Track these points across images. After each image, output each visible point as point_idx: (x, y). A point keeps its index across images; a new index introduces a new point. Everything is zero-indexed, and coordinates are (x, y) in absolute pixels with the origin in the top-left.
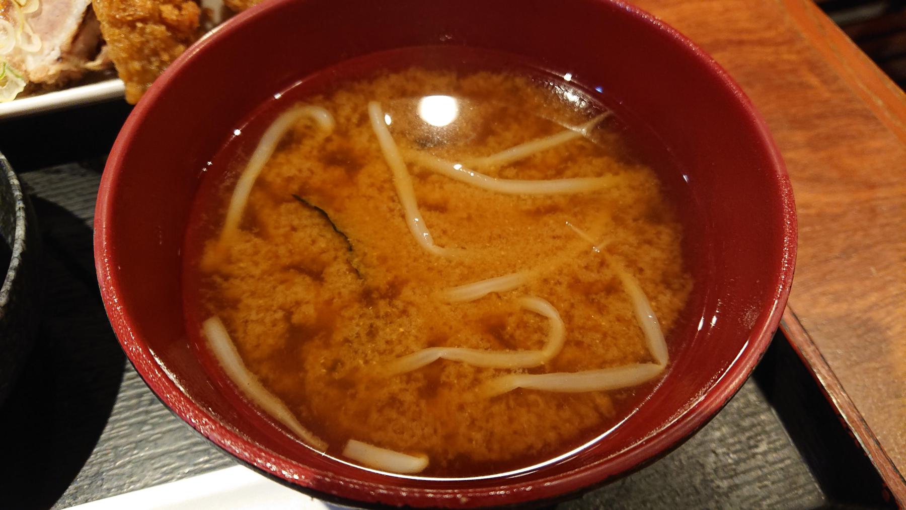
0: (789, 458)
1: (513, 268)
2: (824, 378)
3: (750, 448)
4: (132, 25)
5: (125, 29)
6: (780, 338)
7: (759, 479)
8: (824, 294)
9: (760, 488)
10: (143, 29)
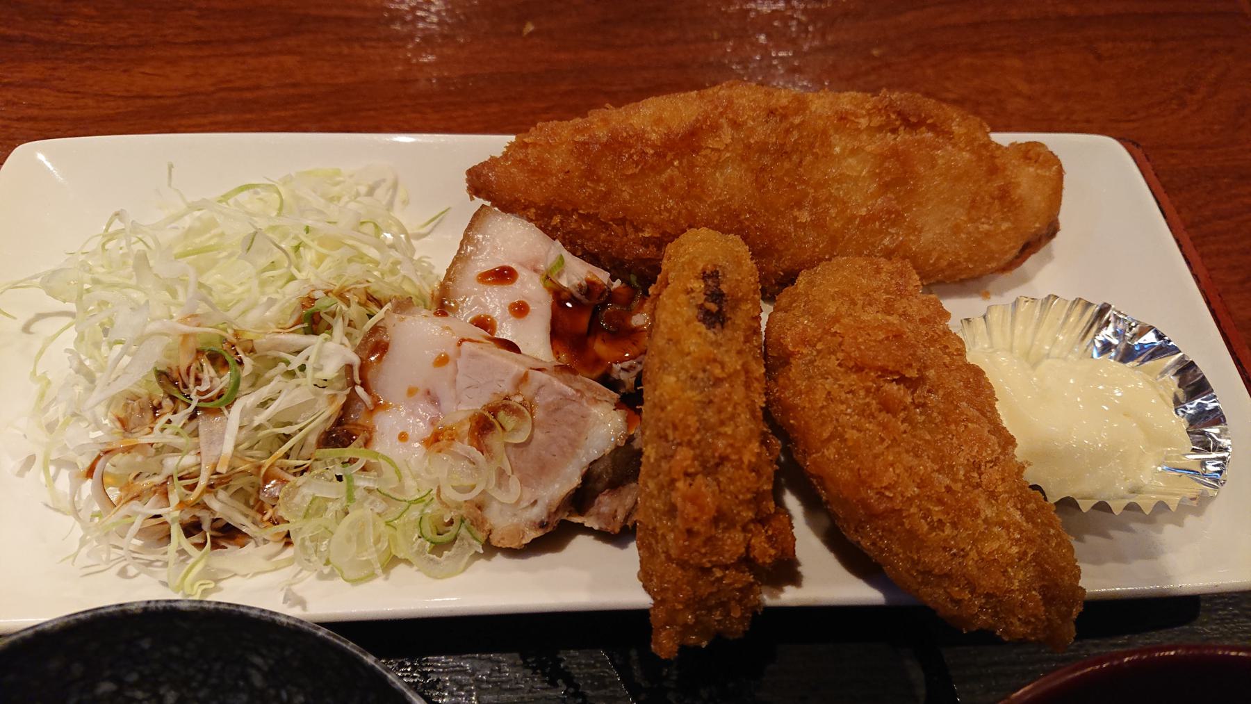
4: (706, 571)
10: (720, 580)
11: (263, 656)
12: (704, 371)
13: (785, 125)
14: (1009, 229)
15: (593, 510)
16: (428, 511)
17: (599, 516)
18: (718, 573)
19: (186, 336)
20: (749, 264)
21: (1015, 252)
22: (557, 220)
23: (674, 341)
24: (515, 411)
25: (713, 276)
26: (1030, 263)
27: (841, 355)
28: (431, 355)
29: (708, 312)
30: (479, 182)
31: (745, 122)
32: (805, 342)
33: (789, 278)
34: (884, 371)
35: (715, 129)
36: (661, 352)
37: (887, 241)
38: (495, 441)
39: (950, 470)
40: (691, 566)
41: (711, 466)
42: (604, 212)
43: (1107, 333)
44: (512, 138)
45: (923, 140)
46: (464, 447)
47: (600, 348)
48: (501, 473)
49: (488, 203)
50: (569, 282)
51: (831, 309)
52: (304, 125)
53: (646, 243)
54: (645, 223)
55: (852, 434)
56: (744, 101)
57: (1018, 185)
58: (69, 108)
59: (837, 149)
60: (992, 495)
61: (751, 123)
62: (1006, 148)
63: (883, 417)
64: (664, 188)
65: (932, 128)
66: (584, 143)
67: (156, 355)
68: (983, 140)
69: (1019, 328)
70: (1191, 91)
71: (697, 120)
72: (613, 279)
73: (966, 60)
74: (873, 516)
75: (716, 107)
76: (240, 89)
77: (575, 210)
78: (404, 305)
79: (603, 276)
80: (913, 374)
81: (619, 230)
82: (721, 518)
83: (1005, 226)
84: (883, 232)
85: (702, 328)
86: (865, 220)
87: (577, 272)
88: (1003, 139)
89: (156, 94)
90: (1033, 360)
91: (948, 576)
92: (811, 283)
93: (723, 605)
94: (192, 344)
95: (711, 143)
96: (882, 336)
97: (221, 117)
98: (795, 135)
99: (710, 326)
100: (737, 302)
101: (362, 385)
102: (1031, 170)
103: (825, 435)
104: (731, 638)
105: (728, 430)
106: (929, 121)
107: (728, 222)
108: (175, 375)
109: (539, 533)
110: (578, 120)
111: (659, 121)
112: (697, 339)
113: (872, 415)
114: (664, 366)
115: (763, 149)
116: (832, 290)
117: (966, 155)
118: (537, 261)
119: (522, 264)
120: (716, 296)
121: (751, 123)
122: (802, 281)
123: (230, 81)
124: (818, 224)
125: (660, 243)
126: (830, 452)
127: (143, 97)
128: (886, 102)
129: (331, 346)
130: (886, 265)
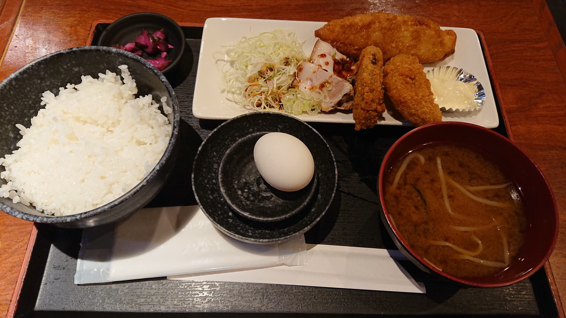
0: (531, 299)
1: (473, 225)
2: (551, 280)
3: (520, 292)
4: (368, 111)
5: (366, 112)
6: (543, 270)
7: (520, 301)
8: (561, 253)
9: (520, 303)
10: (371, 113)
11: (281, 125)
12: (372, 73)
13: (391, 23)
14: (441, 51)
15: (342, 106)
16: (311, 102)
17: (344, 107)
18: (371, 112)
19: (266, 64)
20: (381, 53)
21: (443, 56)
22: (335, 43)
23: (366, 67)
24: (330, 83)
25: (374, 55)
26: (447, 59)
27: (399, 73)
28: (312, 71)
29: (373, 62)
30: (317, 34)
31: (382, 22)
32: (392, 70)
33: (389, 59)
34: (407, 76)
35: (375, 23)
36: (363, 69)
37: (412, 52)
38: (325, 89)
39: (418, 96)
40: (366, 110)
41: (372, 91)
42: (347, 42)
43: (462, 76)
44: (326, 23)
45: (423, 28)
46: (318, 90)
47: (344, 73)
48: (325, 96)
49: (319, 39)
50: (338, 58)
51: (398, 64)
52: (232, 14)
53: (355, 50)
54: (356, 45)
55: (399, 87)
56: (382, 17)
57: (445, 40)
58: (203, 8)
59: (403, 29)
60: (426, 102)
61: (383, 22)
62: (444, 31)
63: (406, 85)
64: (361, 37)
65: (426, 25)
66: (343, 25)
67: (259, 68)
68: (438, 29)
69: (441, 74)
70: (505, 17)
71: (371, 21)
72: (347, 58)
73: (442, 5)
74: (401, 103)
75: (375, 18)
76: (247, 6)
77: (340, 41)
78: (305, 60)
79: (345, 57)
80: (413, 77)
81: (350, 47)
82: (373, 101)
83: (440, 50)
84: (412, 50)
85: (372, 65)
86: (407, 46)
87: (339, 56)
88: (443, 28)
89: (225, 6)
90: (443, 81)
91: (414, 115)
92: (394, 59)
93: (370, 119)
94: (266, 66)
95: (374, 26)
96: (407, 69)
97: (243, 14)
98: (393, 25)
99: (374, 65)
100: (379, 61)
101: (298, 77)
102: (449, 37)
103: (394, 88)
104: (370, 128)
105: (376, 84)
106: (425, 24)
107: (376, 45)
108: (262, 72)
109: (332, 108)
110: (342, 19)
111: (361, 20)
112: (371, 67)
113: (404, 84)
114: (364, 72)
115: (385, 28)
116: (398, 60)
117: (433, 32)
118: (330, 53)
119: (327, 53)
120: (375, 59)
121: (383, 22)
122: (392, 59)
123: (243, 3)
124: (397, 47)
125: (360, 50)
126: (394, 91)
127: (223, 6)
128: (416, 18)
129: (291, 68)
130: (411, 57)
